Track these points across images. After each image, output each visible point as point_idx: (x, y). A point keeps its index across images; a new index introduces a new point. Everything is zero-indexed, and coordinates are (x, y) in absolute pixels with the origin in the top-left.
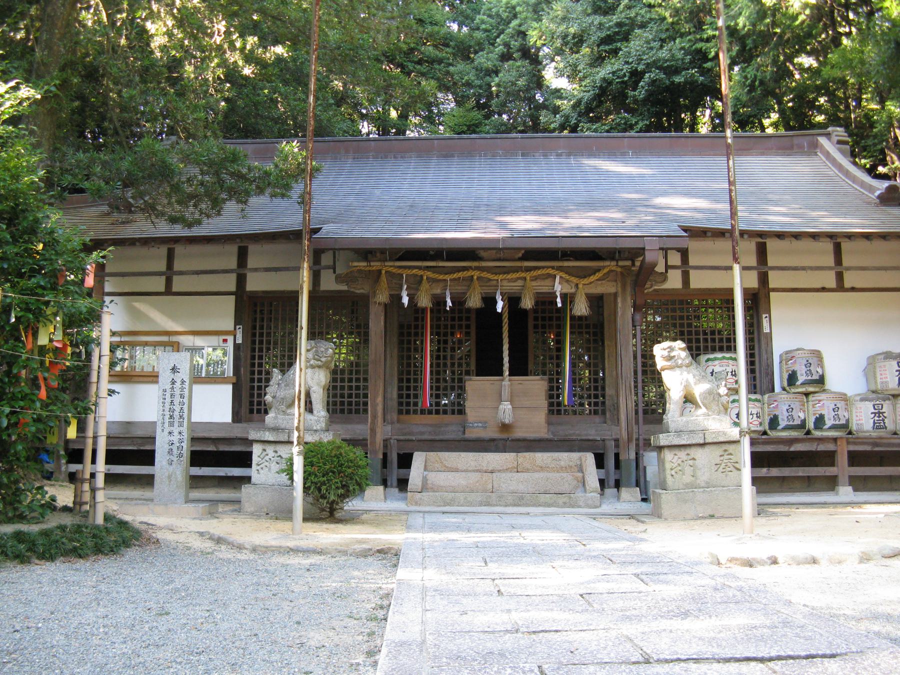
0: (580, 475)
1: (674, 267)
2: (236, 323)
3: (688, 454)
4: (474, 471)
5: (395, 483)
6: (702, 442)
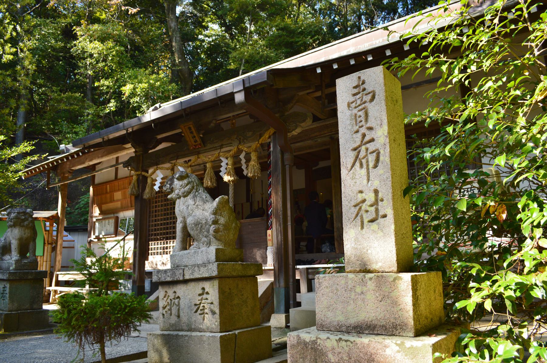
6: (181, 279)
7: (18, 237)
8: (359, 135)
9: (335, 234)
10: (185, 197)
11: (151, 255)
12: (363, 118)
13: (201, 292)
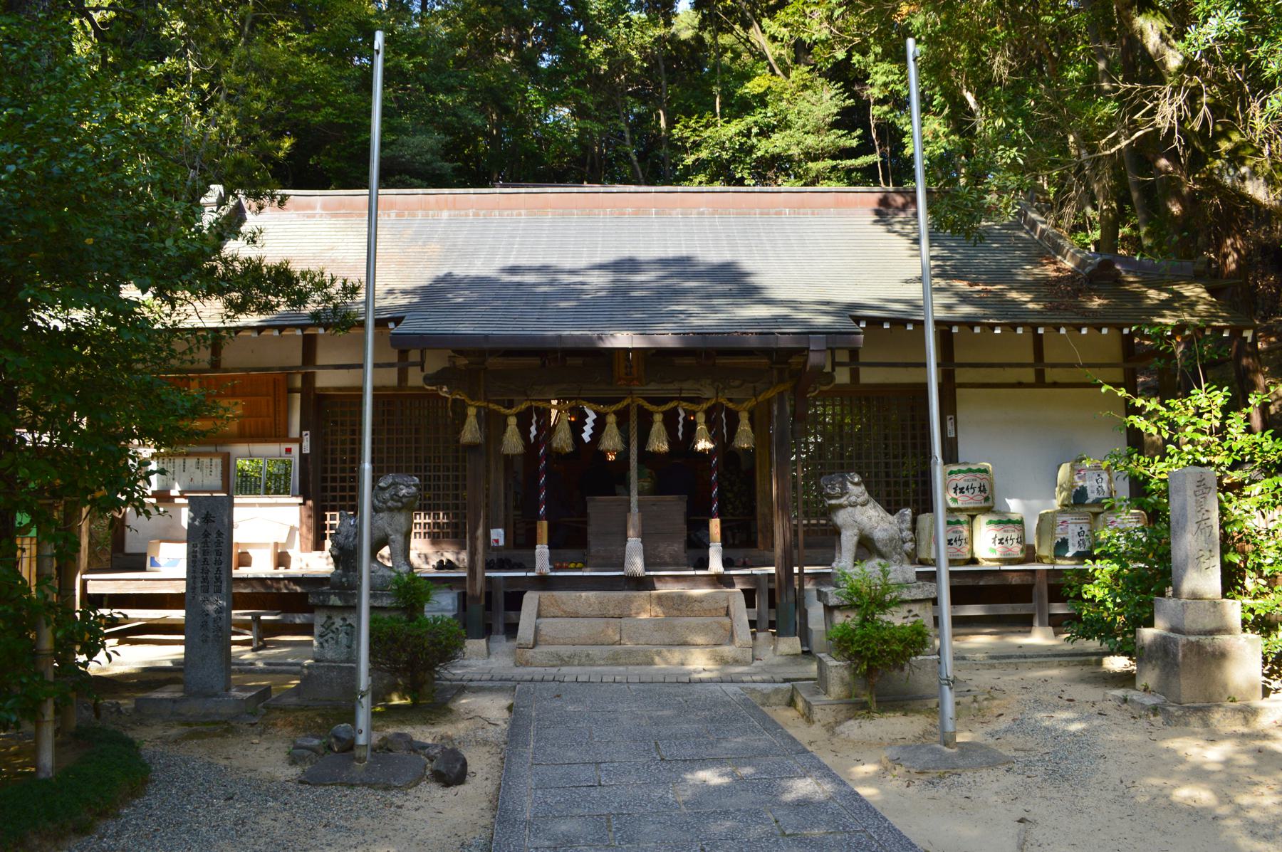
0: (726, 621)
1: (842, 364)
4: (598, 617)
5: (501, 628)
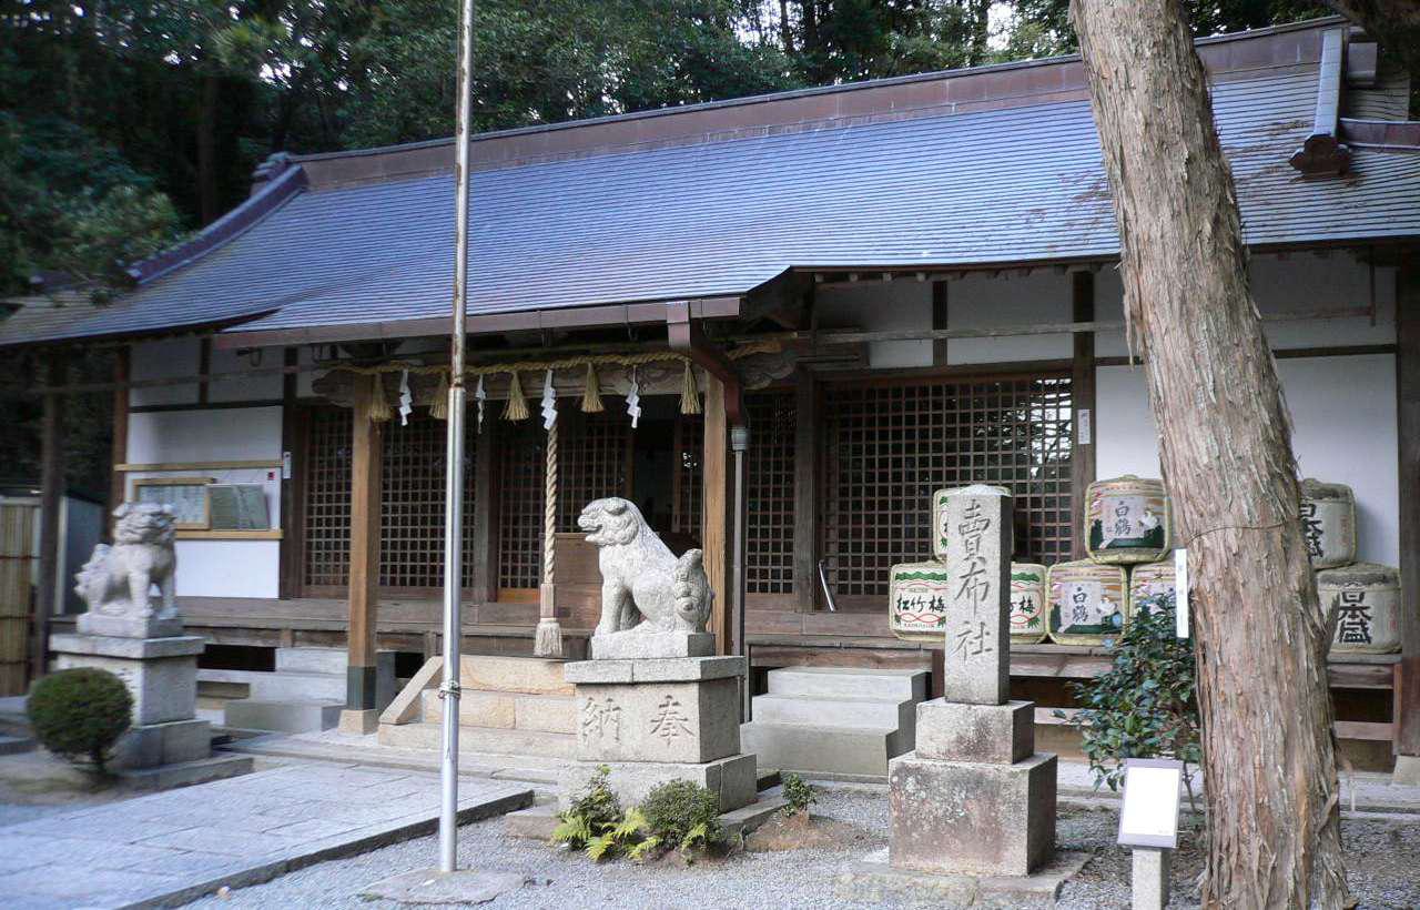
2: (285, 449)
3: (610, 700)
6: (627, 680)
7: (148, 565)
8: (970, 562)
9: (649, 343)
10: (624, 544)
11: (317, 583)
12: (974, 546)
13: (665, 702)
